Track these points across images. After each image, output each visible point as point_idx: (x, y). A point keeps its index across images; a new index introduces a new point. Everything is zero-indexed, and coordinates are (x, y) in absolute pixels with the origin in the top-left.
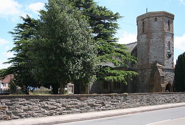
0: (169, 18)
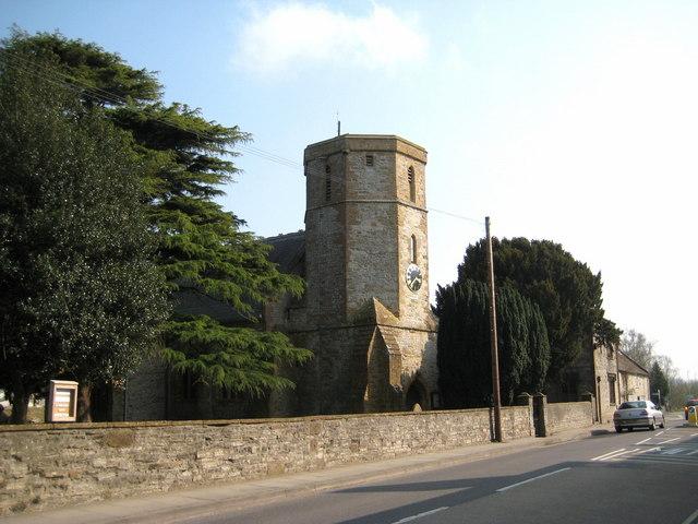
0: (381, 150)
